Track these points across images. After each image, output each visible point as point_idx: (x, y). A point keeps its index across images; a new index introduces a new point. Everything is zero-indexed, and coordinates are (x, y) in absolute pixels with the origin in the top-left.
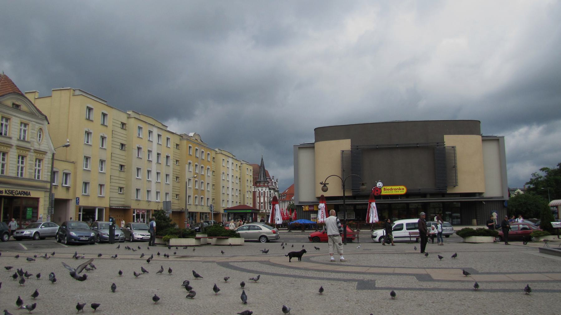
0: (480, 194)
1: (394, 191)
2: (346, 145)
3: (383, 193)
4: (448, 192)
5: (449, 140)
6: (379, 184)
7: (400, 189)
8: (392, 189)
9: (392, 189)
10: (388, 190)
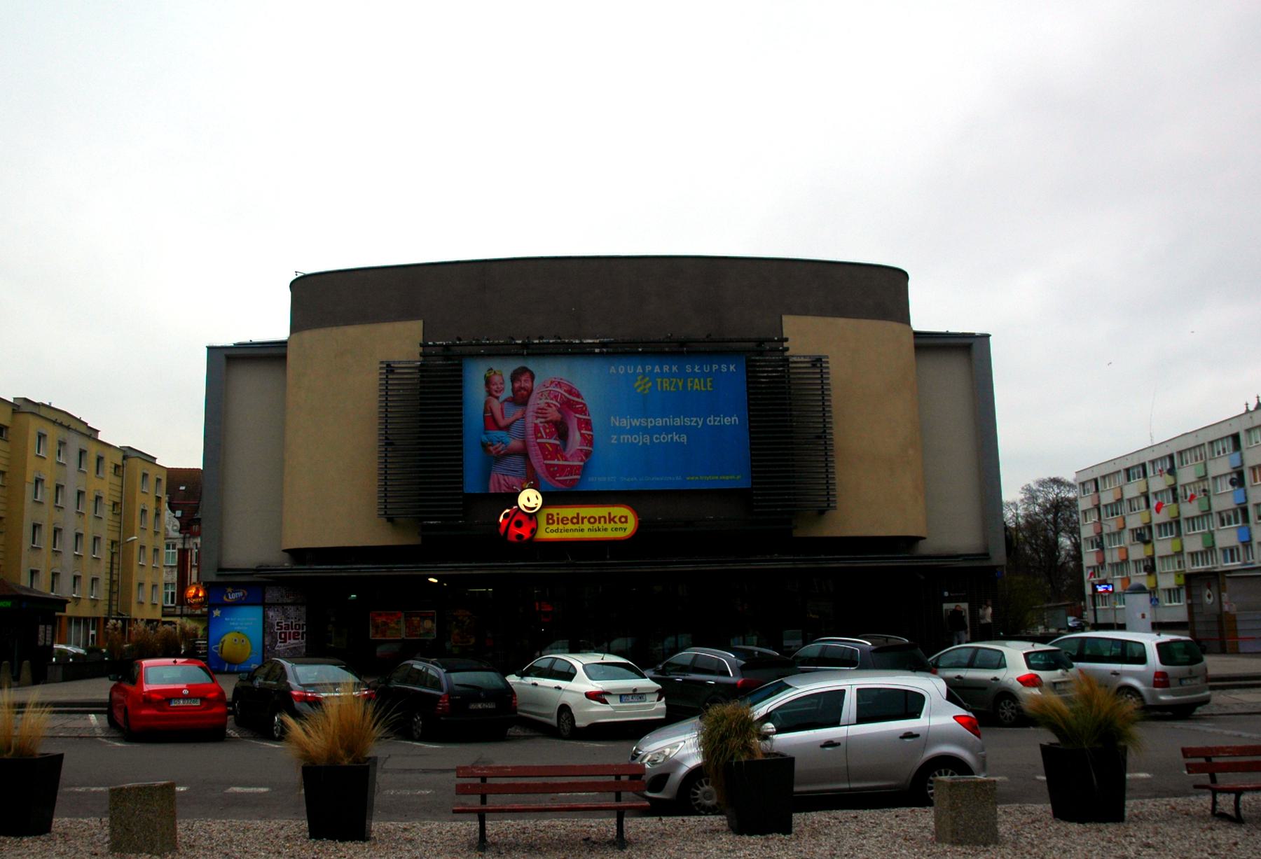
0: (912, 541)
1: (586, 525)
2: (402, 341)
3: (547, 533)
4: (798, 533)
5: (803, 335)
6: (529, 499)
7: (612, 520)
8: (578, 519)
9: (578, 519)
10: (564, 520)
